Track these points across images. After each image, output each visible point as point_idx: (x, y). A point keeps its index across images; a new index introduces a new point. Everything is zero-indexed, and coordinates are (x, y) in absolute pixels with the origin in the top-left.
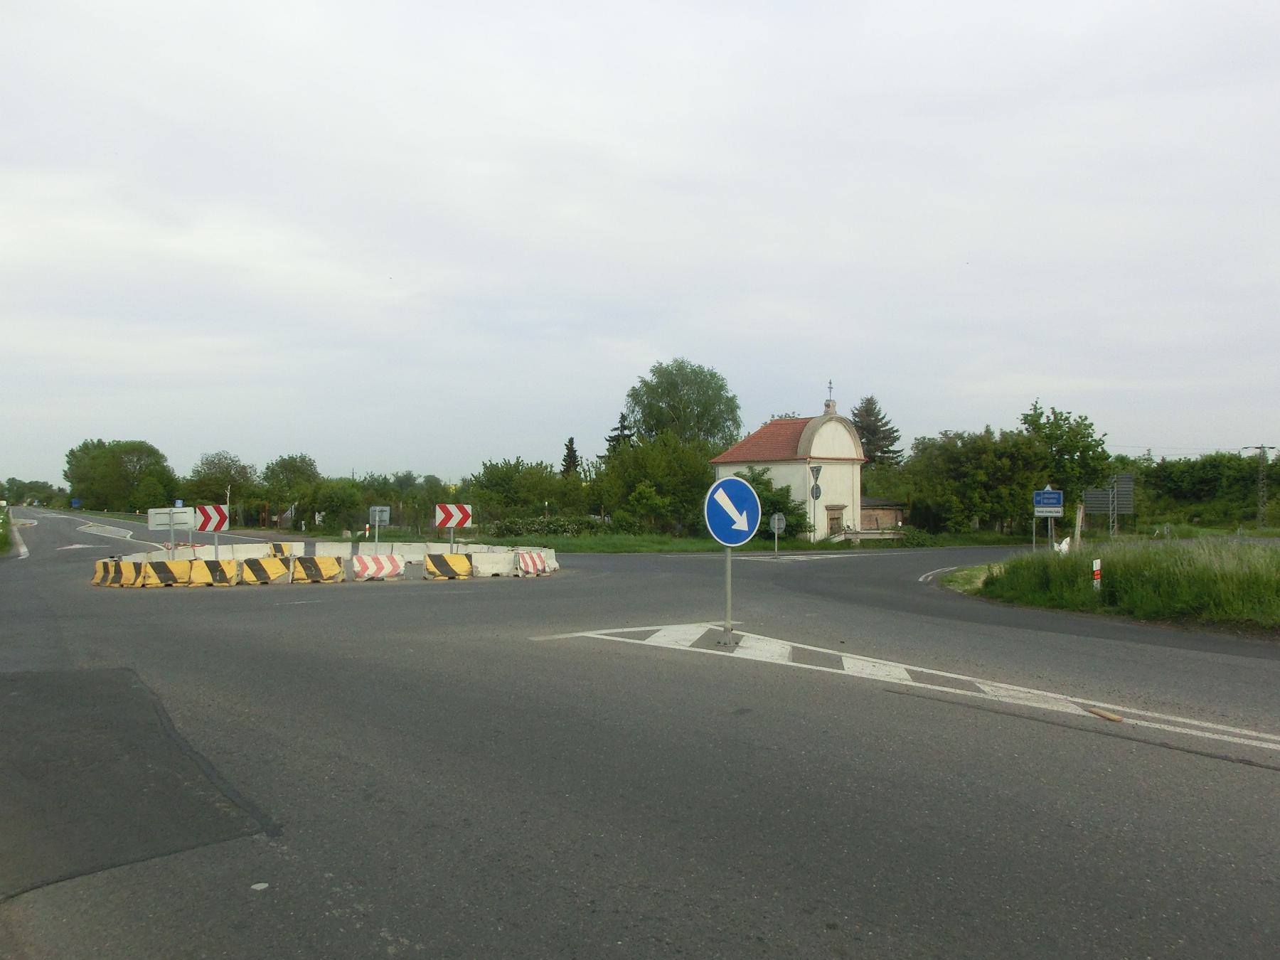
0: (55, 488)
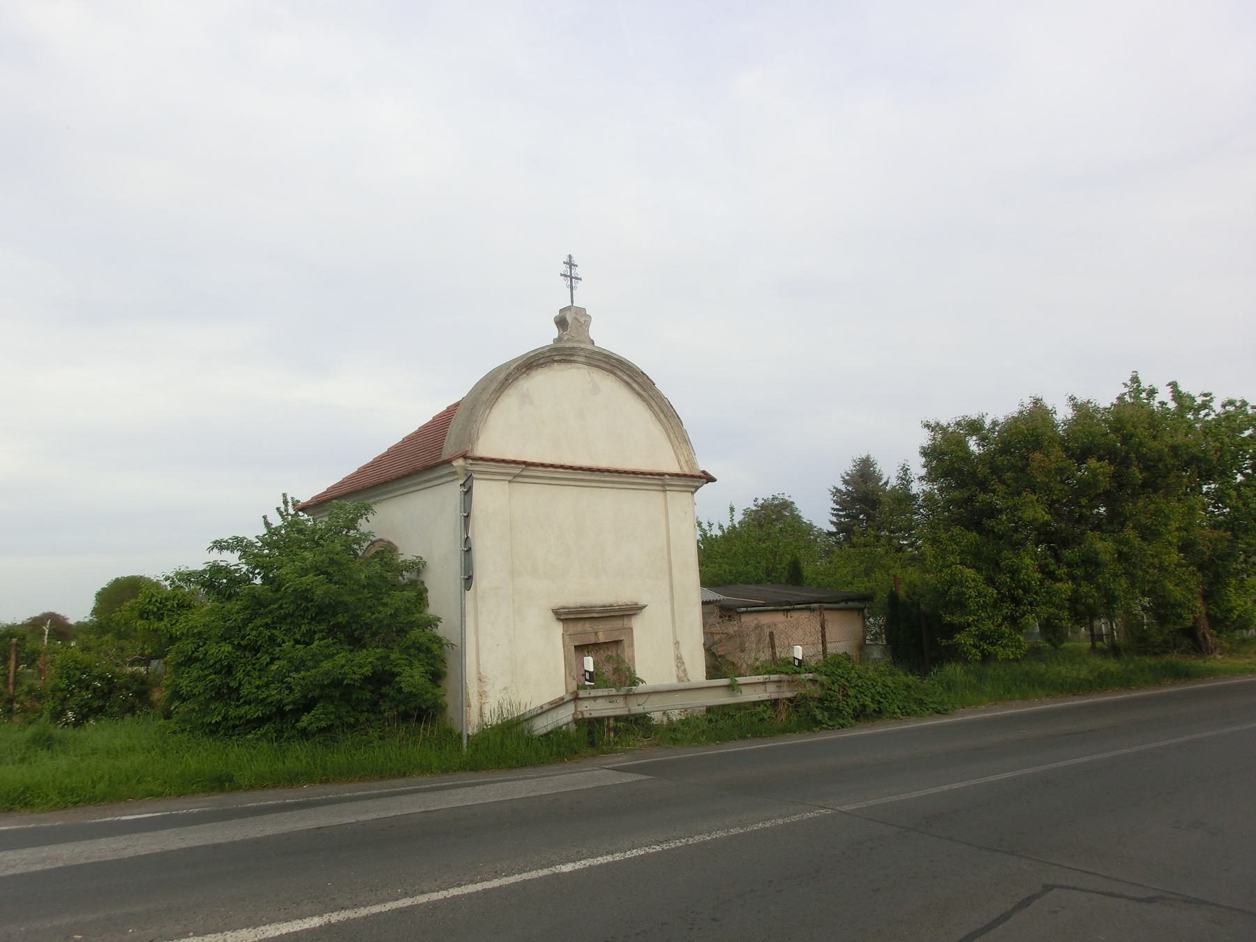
0: (79, 610)
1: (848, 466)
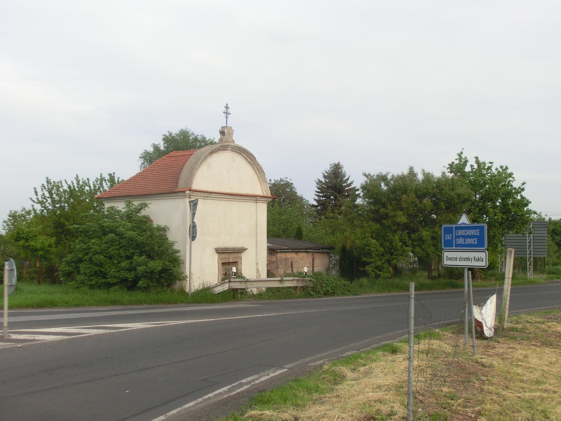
1: (327, 167)
